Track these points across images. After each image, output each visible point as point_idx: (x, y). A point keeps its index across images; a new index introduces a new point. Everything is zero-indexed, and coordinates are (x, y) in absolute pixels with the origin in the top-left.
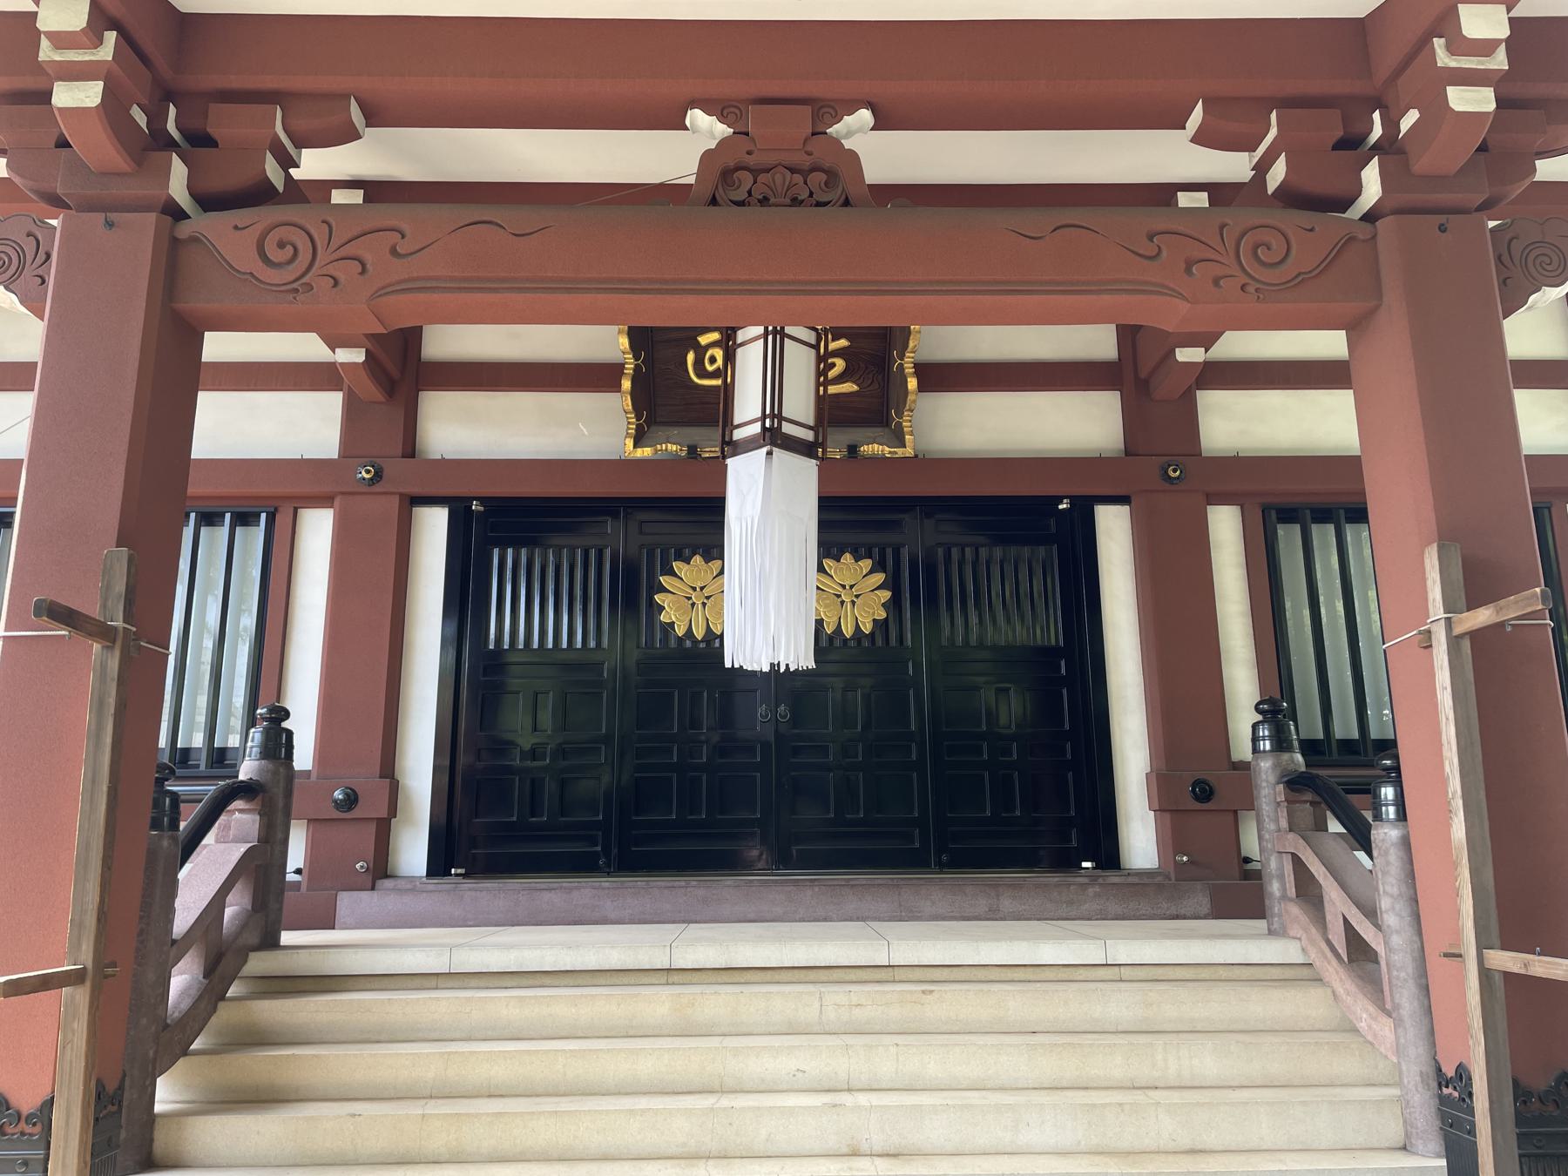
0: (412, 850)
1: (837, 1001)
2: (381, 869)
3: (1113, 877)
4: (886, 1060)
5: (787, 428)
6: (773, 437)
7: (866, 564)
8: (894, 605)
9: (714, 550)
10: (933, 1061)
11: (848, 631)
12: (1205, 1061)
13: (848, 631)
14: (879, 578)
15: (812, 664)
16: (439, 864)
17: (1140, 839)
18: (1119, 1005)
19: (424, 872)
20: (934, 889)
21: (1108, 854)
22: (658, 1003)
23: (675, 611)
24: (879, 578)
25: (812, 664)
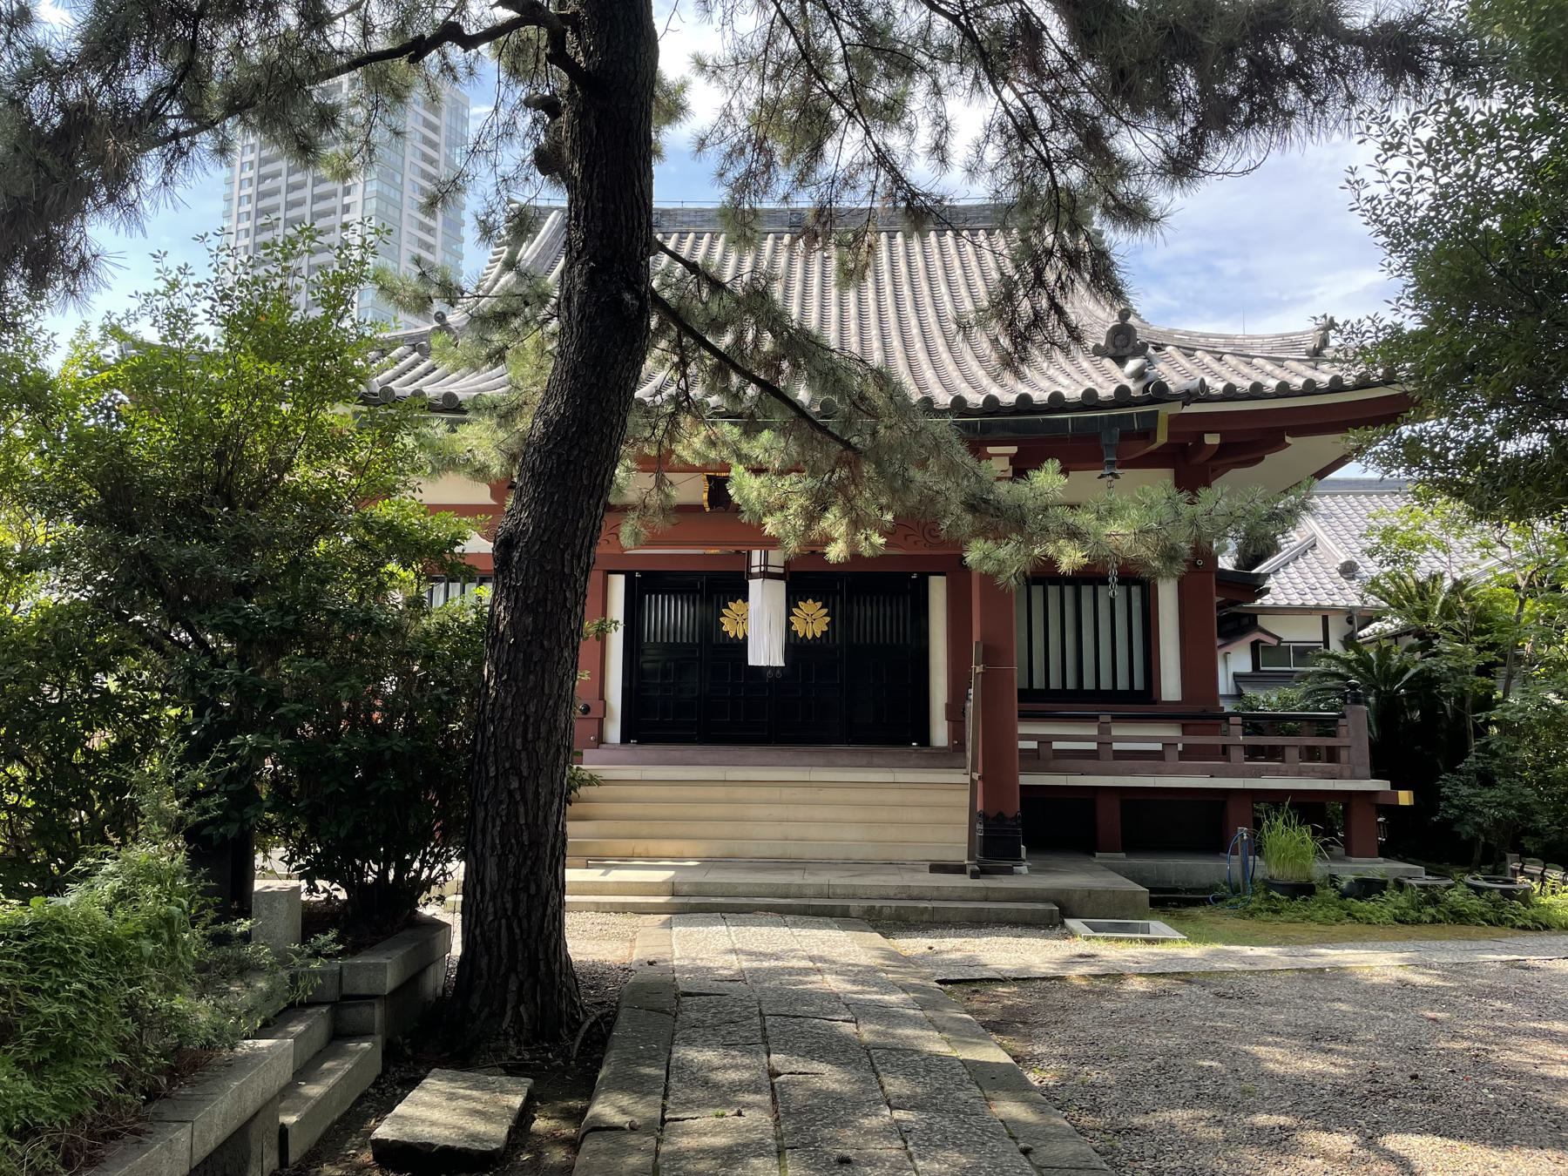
0: (614, 732)
1: (787, 793)
2: (600, 740)
3: (926, 750)
4: (802, 812)
5: (770, 569)
6: (766, 575)
7: (819, 604)
8: (831, 624)
9: (746, 599)
10: (818, 813)
11: (809, 636)
12: (917, 815)
13: (809, 636)
14: (825, 611)
15: (779, 662)
16: (625, 739)
17: (940, 733)
18: (894, 796)
19: (618, 741)
20: (752, 752)
21: (924, 737)
22: (719, 792)
23: (729, 626)
24: (825, 611)
25: (779, 662)
